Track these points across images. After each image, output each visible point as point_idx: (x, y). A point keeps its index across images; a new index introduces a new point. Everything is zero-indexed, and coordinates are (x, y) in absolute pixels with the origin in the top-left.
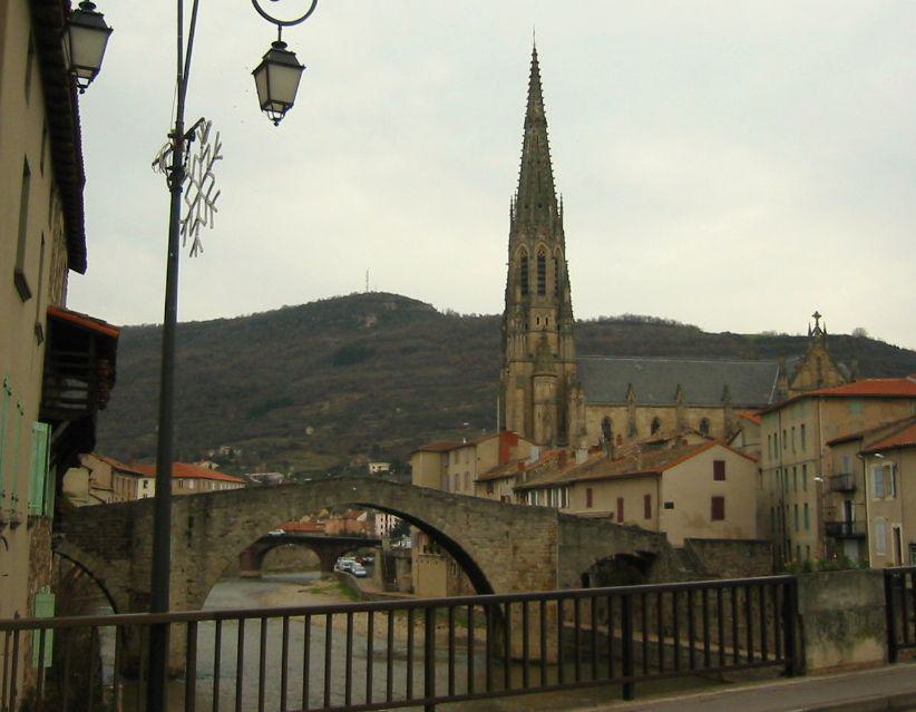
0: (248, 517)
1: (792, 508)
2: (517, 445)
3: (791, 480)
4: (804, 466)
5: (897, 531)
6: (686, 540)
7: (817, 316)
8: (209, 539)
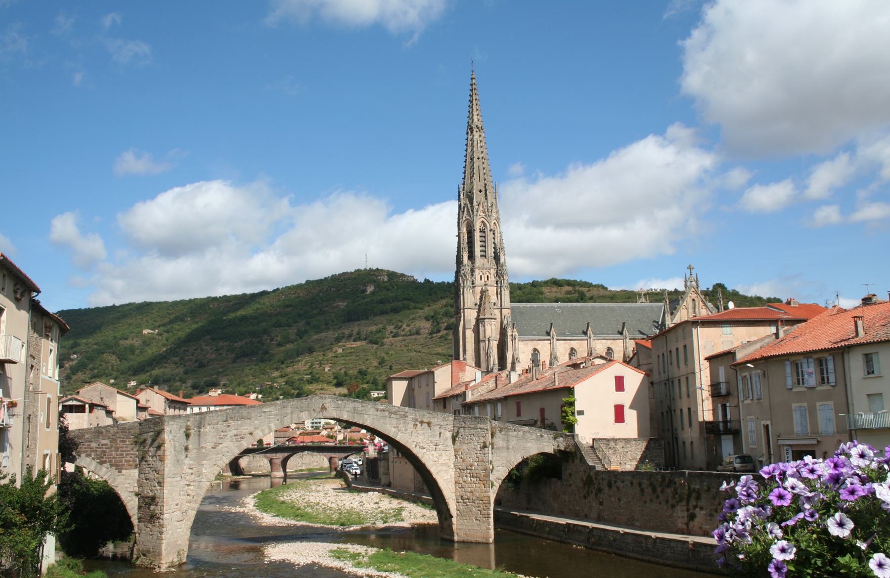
0: (235, 432)
1: (678, 412)
2: (465, 371)
3: (677, 390)
4: (687, 378)
5: (767, 427)
6: (425, 280)
7: (690, 268)
8: (204, 451)
